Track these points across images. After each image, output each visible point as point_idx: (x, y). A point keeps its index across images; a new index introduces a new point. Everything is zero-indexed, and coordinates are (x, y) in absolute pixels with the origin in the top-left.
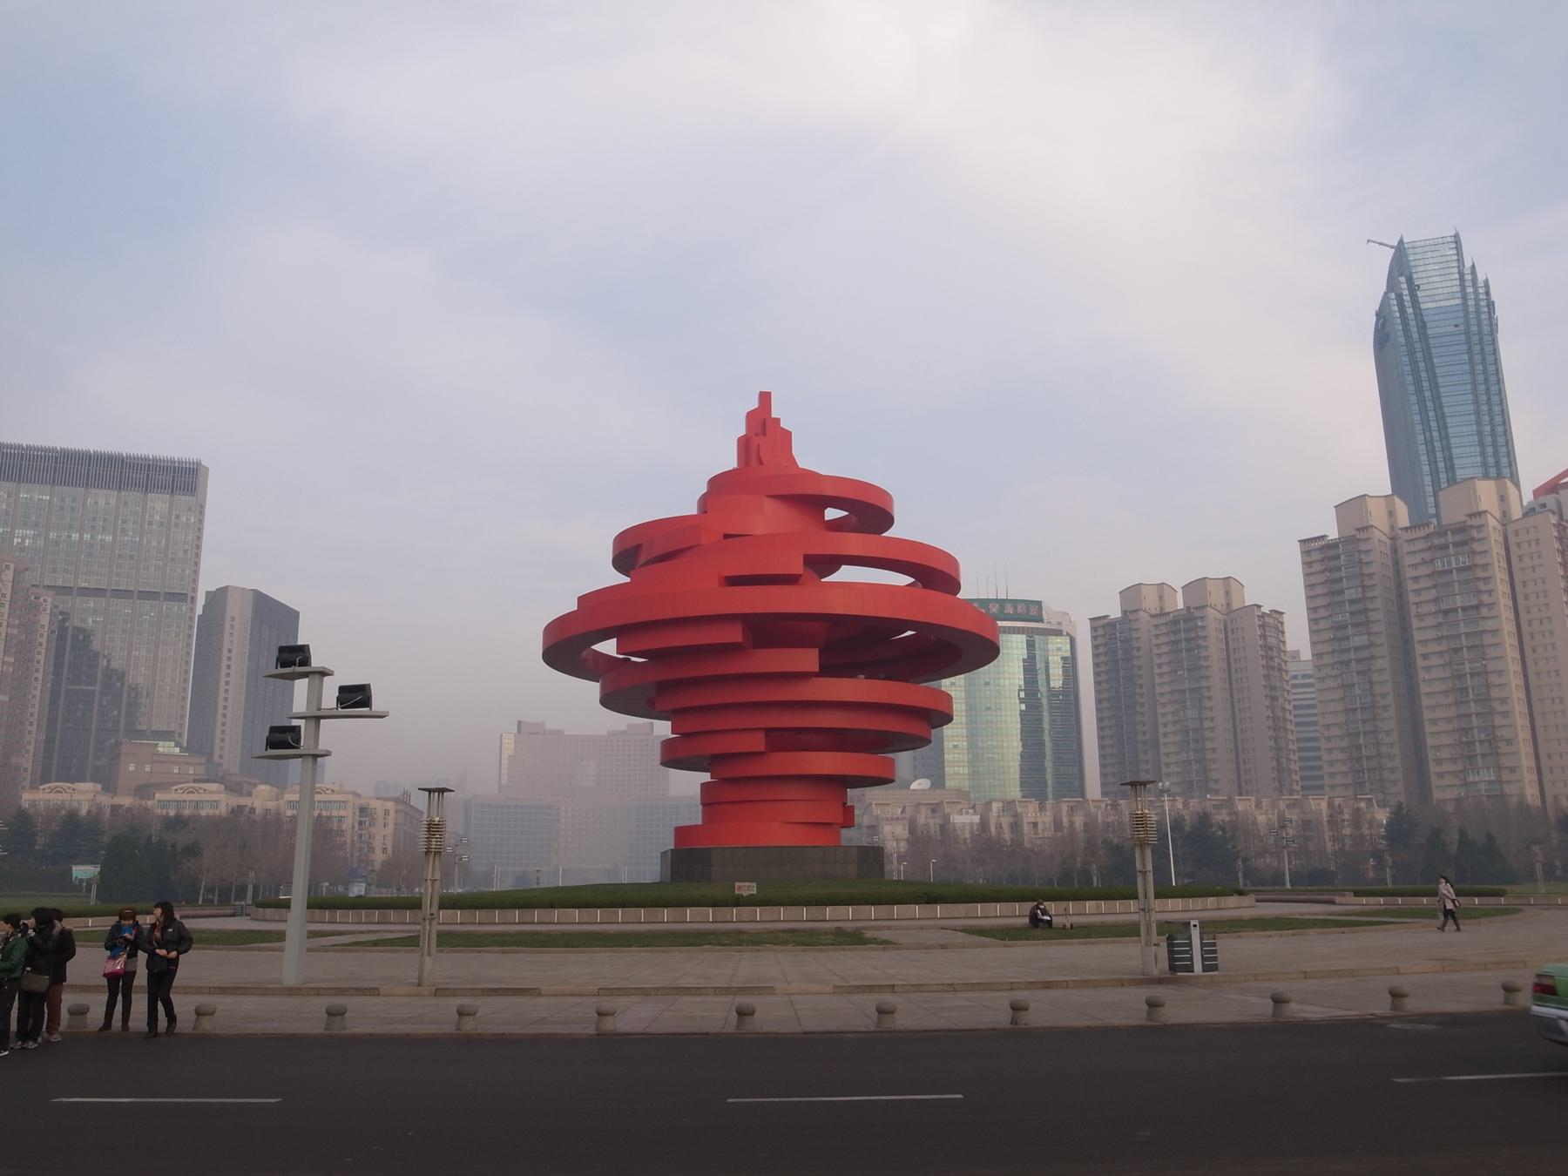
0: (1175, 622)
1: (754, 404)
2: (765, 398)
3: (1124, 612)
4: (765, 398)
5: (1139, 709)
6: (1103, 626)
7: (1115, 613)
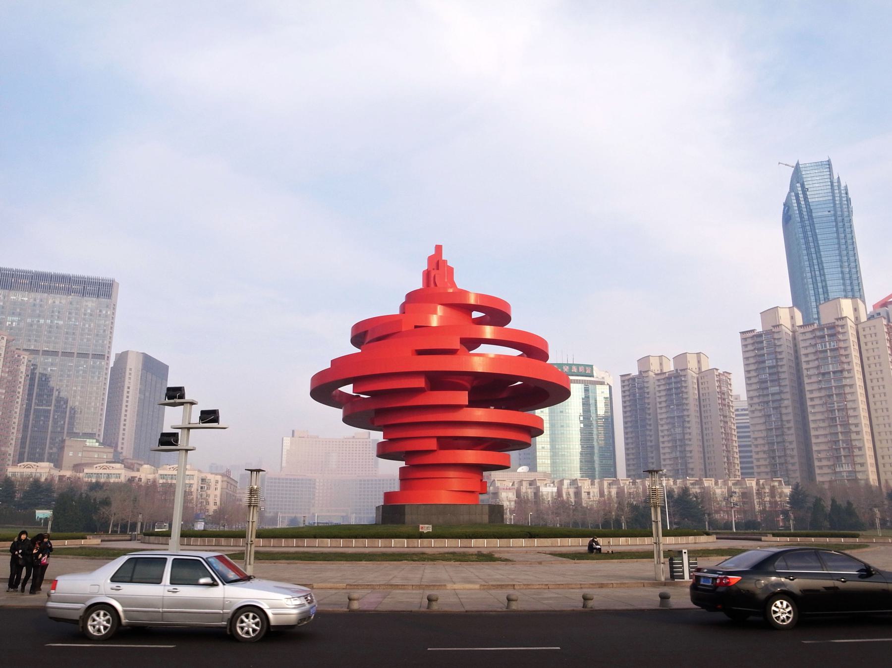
0: (669, 378)
1: (432, 252)
2: (439, 248)
3: (640, 372)
4: (439, 248)
5: (648, 427)
6: (628, 380)
7: (635, 372)
